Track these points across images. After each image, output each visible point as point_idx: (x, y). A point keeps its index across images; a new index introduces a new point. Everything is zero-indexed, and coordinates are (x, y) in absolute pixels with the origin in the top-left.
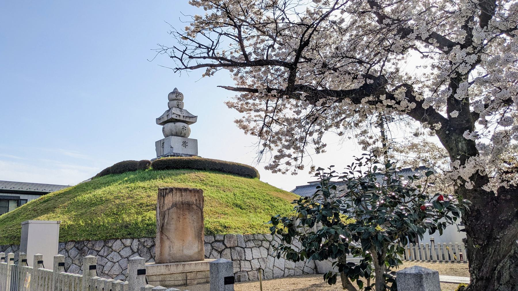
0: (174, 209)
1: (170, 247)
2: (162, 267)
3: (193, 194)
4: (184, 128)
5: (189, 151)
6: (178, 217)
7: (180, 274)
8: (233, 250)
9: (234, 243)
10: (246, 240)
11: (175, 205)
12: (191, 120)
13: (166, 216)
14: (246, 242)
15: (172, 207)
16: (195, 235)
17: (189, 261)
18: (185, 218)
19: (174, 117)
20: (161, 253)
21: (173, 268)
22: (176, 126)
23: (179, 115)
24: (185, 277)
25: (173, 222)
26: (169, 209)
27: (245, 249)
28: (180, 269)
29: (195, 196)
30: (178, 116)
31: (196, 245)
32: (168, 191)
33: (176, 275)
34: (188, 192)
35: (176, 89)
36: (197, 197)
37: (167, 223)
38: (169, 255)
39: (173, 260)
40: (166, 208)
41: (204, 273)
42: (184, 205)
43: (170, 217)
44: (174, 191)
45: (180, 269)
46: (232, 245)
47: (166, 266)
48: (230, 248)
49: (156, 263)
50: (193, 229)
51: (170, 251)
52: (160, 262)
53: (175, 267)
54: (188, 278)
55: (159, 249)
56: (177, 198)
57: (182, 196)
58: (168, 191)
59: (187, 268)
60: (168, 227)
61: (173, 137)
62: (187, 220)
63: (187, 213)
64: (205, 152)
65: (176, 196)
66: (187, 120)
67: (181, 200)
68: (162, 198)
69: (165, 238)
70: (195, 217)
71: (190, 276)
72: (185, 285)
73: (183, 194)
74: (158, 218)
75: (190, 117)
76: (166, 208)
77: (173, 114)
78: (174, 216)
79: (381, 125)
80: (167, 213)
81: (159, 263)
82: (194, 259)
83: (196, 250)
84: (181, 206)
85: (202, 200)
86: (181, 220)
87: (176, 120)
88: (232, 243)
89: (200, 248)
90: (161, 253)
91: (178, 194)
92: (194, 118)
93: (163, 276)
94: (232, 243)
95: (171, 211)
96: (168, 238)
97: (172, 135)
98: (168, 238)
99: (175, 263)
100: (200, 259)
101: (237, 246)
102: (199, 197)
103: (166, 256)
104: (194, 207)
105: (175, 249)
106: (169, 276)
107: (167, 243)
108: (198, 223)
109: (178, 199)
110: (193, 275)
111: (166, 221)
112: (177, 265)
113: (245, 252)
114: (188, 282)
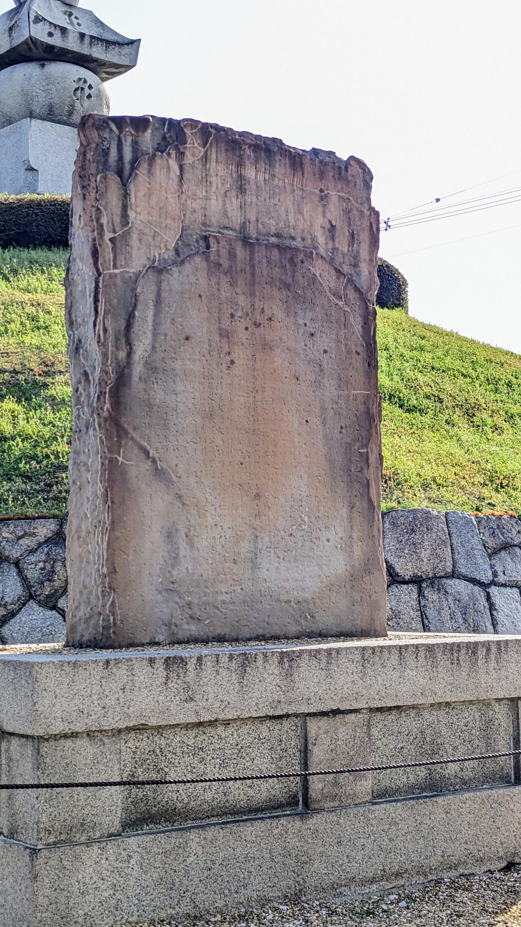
0: (192, 275)
1: (170, 535)
2: (142, 673)
3: (312, 187)
4: (81, 88)
6: (225, 334)
7: (264, 729)
8: (431, 595)
9: (434, 554)
10: (491, 543)
11: (199, 243)
12: (111, 56)
13: (145, 316)
14: (493, 553)
15: (180, 256)
16: (331, 462)
17: (298, 637)
18: (266, 346)
19: (40, 33)
20: (112, 578)
21: (218, 686)
22: (49, 80)
23: (63, 30)
24: (294, 744)
25: (189, 362)
26: (158, 269)
27: (493, 590)
28: (265, 687)
29: (324, 198)
30: (57, 33)
31: (337, 532)
32: (148, 139)
33: (230, 735)
34: (281, 168)
36: (334, 211)
37: (152, 368)
38: (170, 588)
39: (193, 629)
40: (137, 260)
41: (410, 723)
42: (260, 254)
43: (166, 325)
44: (194, 148)
45: (265, 687)
46: (426, 568)
47: (168, 662)
48: (416, 581)
49: (75, 644)
50: (315, 421)
51: (175, 559)
52: (105, 638)
53: (228, 677)
54: (318, 754)
55: (98, 545)
56: (212, 197)
57: (241, 186)
58: (148, 139)
59: (314, 685)
60: (158, 395)
61: (36, 123)
62: (279, 358)
63: (278, 311)
65: (205, 180)
66: (97, 52)
67: (236, 219)
68: (114, 181)
69: (138, 470)
70: (325, 341)
71: (328, 743)
72: (300, 803)
73: (250, 173)
74: (88, 333)
75: (108, 43)
76: (137, 260)
77: (38, 19)
78: (196, 320)
80: (146, 291)
81: (95, 644)
82: (325, 621)
83: (338, 565)
84: (241, 253)
85: (364, 236)
86: (240, 355)
87: (50, 48)
88: (425, 554)
89: (358, 550)
90: (112, 578)
91: (220, 170)
92: (126, 50)
93: (144, 743)
94: (425, 554)
95: (176, 280)
96: (159, 473)
97: (31, 115)
98: (159, 473)
99: (227, 648)
100: (361, 623)
101: (454, 575)
102: (348, 212)
103: (147, 599)
104: (319, 269)
105: (203, 544)
106: (191, 738)
107: (152, 506)
108: (343, 383)
109: (215, 205)
110: (345, 730)
111: (142, 347)
112: (246, 661)
113: (492, 607)
114: (317, 786)
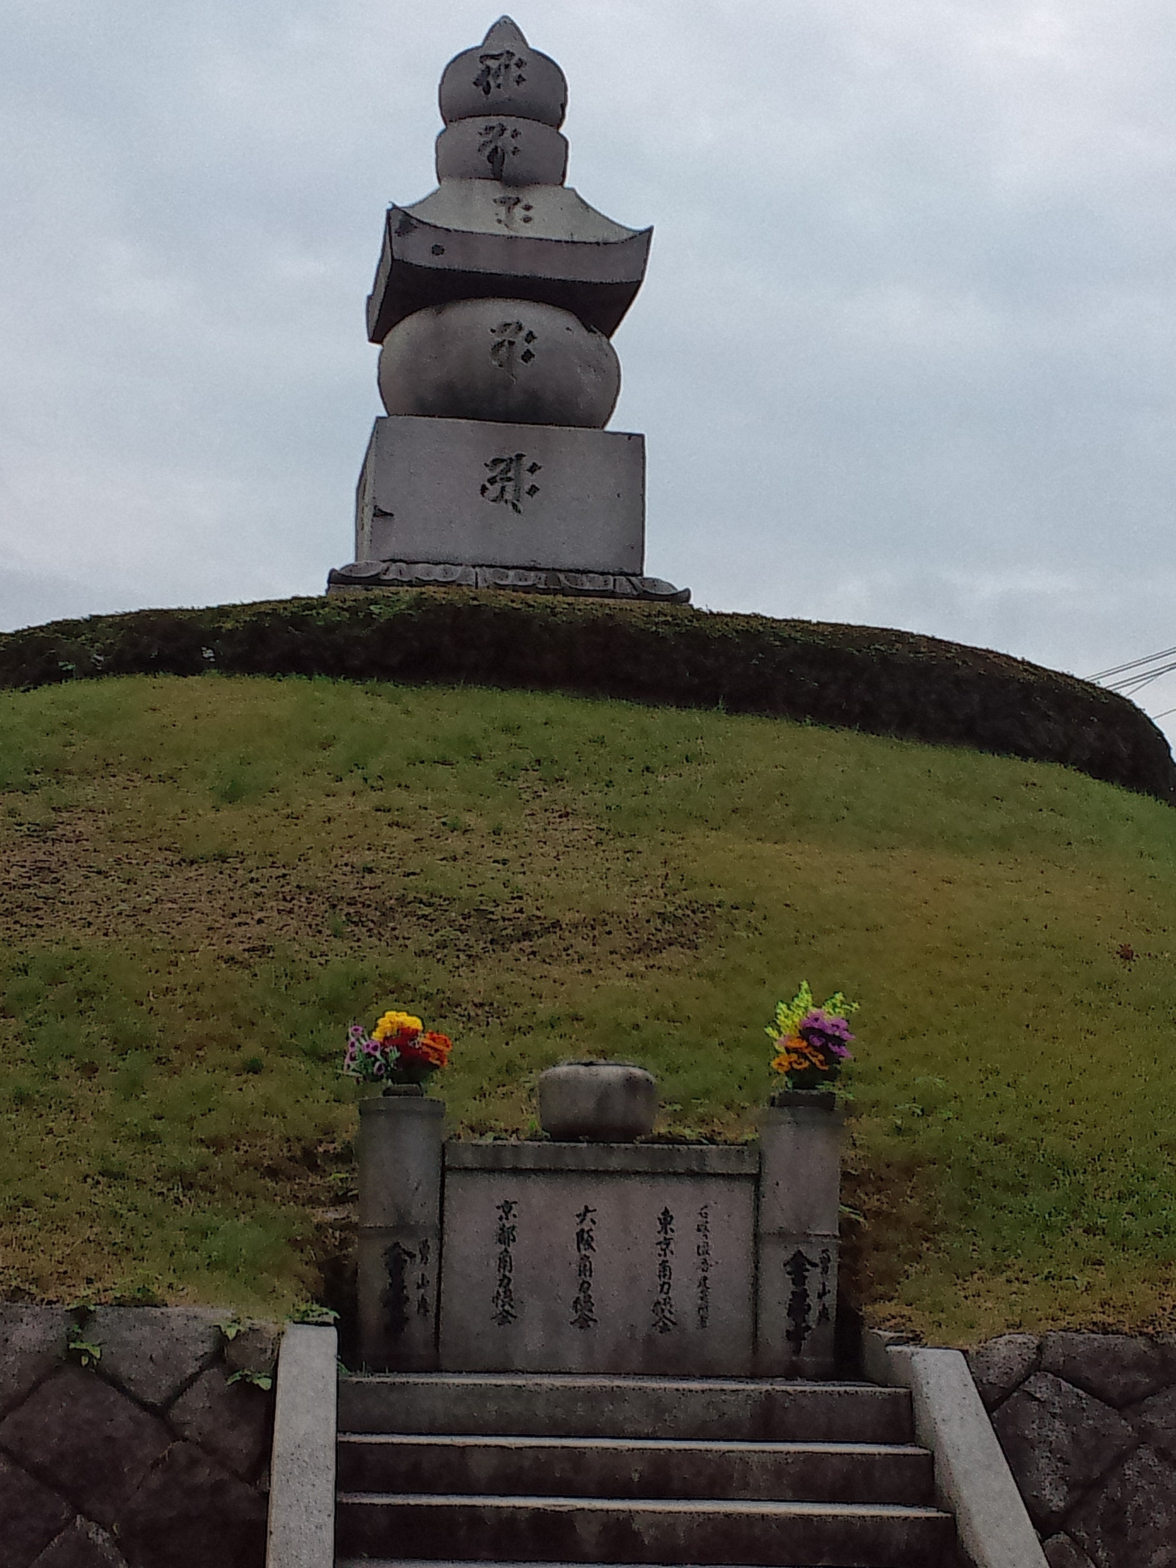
5: (557, 534)
35: (505, 28)
64: (721, 551)
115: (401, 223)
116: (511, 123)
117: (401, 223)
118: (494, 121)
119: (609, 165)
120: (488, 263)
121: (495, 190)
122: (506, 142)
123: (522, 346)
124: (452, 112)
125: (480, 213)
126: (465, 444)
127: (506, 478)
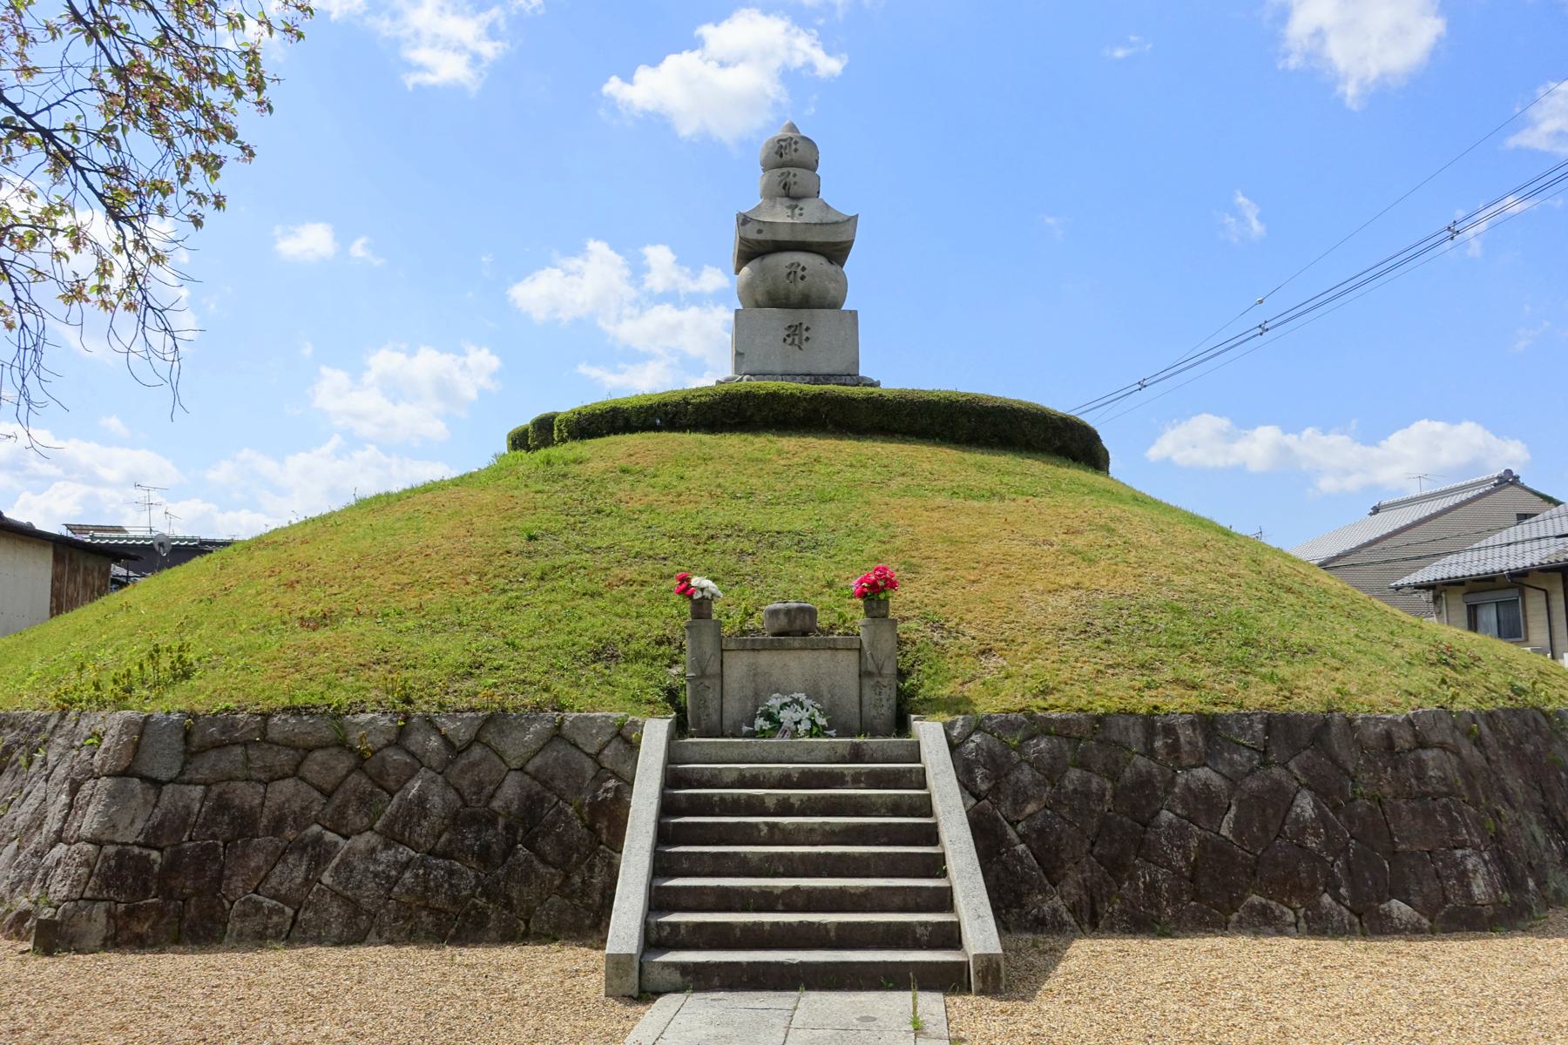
64: (893, 363)
79: (595, 757)
115: (744, 220)
116: (792, 170)
117: (744, 220)
118: (785, 170)
119: (838, 189)
120: (784, 236)
121: (787, 202)
122: (791, 179)
123: (800, 273)
124: (767, 166)
125: (781, 215)
126: (778, 319)
127: (795, 333)
